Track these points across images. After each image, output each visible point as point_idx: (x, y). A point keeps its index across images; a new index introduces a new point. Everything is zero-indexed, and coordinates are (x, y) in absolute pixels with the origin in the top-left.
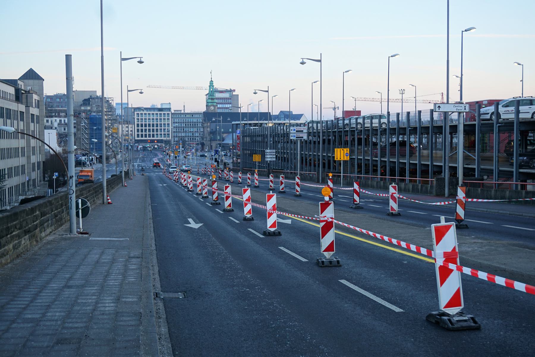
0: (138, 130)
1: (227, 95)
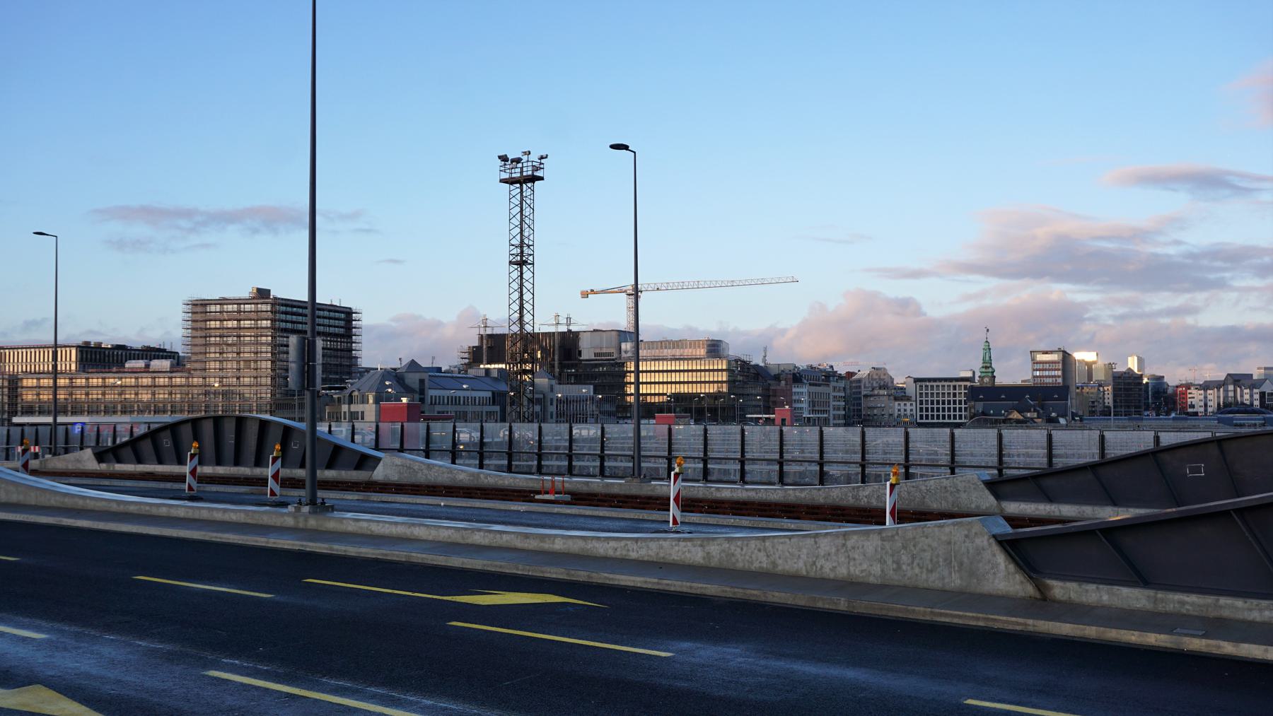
0: (921, 409)
1: (1054, 357)
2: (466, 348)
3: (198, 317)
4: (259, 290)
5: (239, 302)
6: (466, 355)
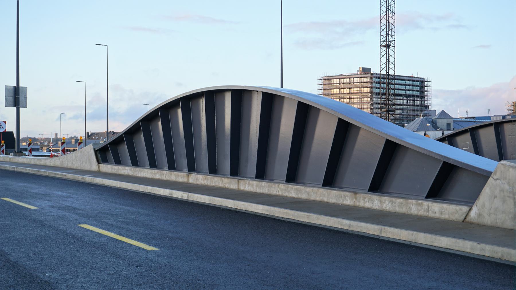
2: (511, 103)
3: (327, 87)
4: (364, 69)
5: (350, 77)
6: (511, 108)
